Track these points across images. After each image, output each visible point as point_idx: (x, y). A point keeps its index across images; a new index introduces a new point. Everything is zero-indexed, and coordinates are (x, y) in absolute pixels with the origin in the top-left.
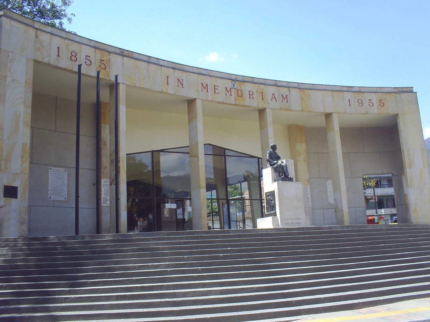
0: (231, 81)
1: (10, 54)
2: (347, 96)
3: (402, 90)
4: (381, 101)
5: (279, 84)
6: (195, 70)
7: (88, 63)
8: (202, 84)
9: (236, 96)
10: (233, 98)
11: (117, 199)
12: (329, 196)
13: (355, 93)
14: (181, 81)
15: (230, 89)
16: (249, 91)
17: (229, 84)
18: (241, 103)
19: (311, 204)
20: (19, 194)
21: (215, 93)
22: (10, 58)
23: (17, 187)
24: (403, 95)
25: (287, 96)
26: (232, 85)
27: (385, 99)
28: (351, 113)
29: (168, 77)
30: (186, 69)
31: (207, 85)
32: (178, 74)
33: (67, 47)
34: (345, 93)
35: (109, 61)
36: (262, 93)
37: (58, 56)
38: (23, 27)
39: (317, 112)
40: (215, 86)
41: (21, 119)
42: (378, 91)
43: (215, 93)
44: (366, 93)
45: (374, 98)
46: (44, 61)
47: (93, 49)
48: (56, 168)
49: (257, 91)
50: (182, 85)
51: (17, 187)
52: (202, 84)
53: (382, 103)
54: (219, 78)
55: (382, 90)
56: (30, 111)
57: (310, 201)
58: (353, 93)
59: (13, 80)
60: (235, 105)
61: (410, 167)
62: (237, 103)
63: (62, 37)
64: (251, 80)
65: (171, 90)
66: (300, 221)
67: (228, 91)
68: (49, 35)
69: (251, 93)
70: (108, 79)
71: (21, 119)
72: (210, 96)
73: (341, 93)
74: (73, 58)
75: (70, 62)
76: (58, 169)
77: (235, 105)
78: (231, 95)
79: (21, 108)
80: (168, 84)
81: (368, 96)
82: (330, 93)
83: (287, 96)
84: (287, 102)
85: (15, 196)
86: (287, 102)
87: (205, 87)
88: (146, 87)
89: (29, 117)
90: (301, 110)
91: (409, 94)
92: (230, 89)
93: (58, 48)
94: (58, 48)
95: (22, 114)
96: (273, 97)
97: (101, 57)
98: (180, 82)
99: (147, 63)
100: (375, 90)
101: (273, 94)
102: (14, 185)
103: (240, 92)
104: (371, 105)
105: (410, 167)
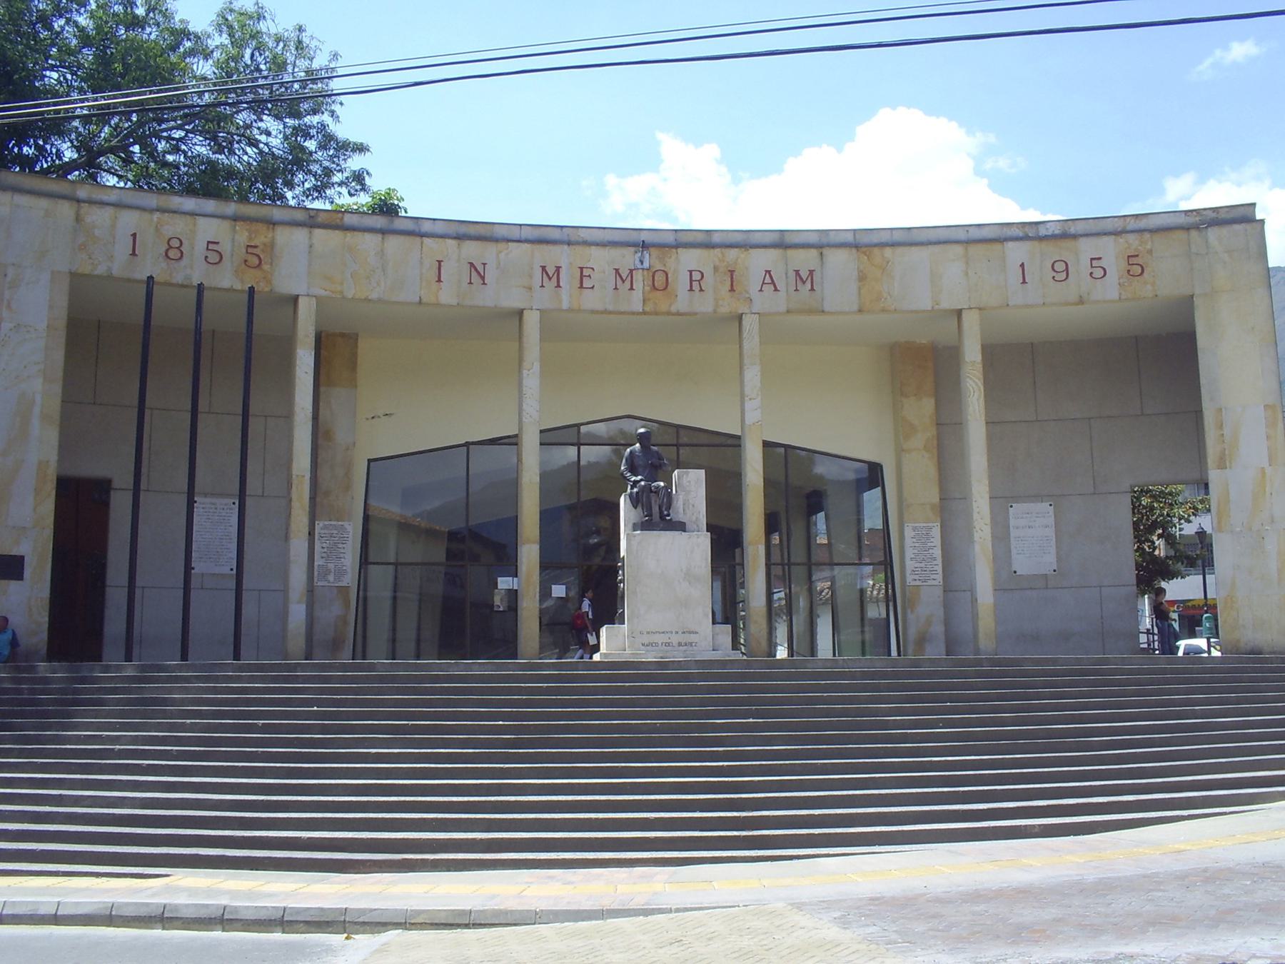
0: (632, 249)
1: (11, 272)
2: (1016, 252)
3: (1214, 215)
4: (1095, 263)
5: (789, 239)
6: (526, 233)
7: (214, 258)
8: (544, 268)
9: (647, 288)
10: (638, 294)
11: (788, 524)
12: (1014, 551)
13: (1044, 244)
14: (480, 269)
15: (631, 271)
16: (691, 272)
17: (628, 259)
18: (663, 307)
19: (939, 577)
20: (28, 572)
21: (581, 287)
22: (8, 279)
23: (22, 558)
24: (1213, 234)
25: (811, 272)
26: (637, 262)
27: (1150, 252)
28: (1027, 306)
29: (440, 262)
30: (501, 232)
31: (558, 269)
32: (472, 250)
33: (157, 229)
34: (1010, 244)
35: (271, 246)
36: (732, 272)
37: (134, 254)
38: (44, 203)
39: (916, 312)
40: (581, 269)
41: (37, 410)
42: (1129, 228)
43: (581, 287)
44: (1082, 241)
45: (1110, 251)
46: (96, 273)
47: (226, 225)
48: (208, 500)
49: (716, 269)
50: (483, 278)
51: (22, 558)
52: (544, 268)
53: (1135, 266)
54: (597, 244)
55: (1142, 224)
56: (57, 388)
57: (939, 569)
58: (1036, 243)
59: (18, 327)
60: (644, 313)
61: (1222, 465)
62: (647, 309)
63: (143, 209)
64: (700, 238)
65: (447, 295)
66: (693, 638)
67: (623, 278)
68: (110, 210)
69: (696, 276)
70: (267, 289)
71: (37, 410)
72: (566, 297)
73: (998, 247)
74: (172, 254)
75: (164, 265)
76: (214, 500)
77: (644, 313)
78: (632, 289)
79: (38, 385)
80: (439, 280)
81: (1088, 248)
82: (959, 249)
83: (811, 272)
84: (812, 289)
85: (18, 575)
86: (812, 289)
87: (552, 275)
88: (374, 296)
89: (56, 404)
90: (855, 308)
91: (1237, 227)
92: (631, 271)
93: (134, 235)
94: (134, 235)
95: (38, 399)
96: (768, 280)
97: (250, 239)
98: (477, 272)
99: (380, 236)
100: (1119, 225)
101: (768, 272)
102: (15, 552)
103: (660, 279)
104: (1099, 273)
105: (1222, 465)
